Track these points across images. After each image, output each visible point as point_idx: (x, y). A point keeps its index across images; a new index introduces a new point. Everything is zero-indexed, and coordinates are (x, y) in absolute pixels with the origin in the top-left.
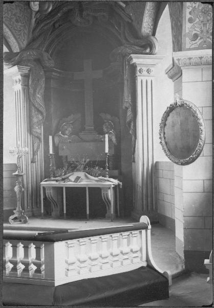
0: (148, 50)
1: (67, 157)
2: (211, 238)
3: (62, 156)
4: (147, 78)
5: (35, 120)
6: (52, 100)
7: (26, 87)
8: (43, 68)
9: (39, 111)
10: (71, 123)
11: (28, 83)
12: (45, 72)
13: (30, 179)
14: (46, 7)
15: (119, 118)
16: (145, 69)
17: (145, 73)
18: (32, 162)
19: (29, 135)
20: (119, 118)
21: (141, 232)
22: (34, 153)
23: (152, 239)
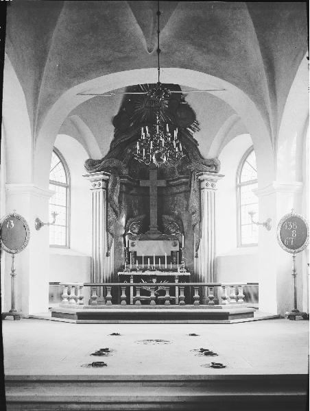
1: (135, 252)
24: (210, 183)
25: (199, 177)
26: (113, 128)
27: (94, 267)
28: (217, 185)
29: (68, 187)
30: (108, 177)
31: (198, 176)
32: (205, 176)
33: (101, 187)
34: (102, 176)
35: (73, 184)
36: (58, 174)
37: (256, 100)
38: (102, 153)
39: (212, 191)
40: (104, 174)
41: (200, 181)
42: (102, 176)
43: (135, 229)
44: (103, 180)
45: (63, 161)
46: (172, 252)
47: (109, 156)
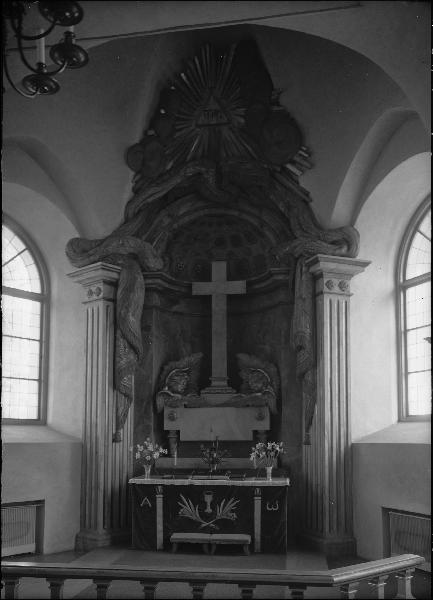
0: (344, 250)
1: (178, 432)
2: (214, 21)
3: (168, 432)
4: (340, 297)
5: (123, 362)
6: (154, 328)
7: (111, 304)
8: (142, 271)
9: (132, 347)
10: (185, 372)
11: (115, 294)
12: (145, 277)
13: (110, 481)
14: (181, 213)
15: (276, 365)
16: (336, 282)
17: (336, 289)
18: (114, 441)
19: (111, 391)
20: (276, 365)
21: (224, 379)
22: (119, 424)
23: (160, 199)
33: (101, 296)
44: (105, 282)
46: (256, 432)
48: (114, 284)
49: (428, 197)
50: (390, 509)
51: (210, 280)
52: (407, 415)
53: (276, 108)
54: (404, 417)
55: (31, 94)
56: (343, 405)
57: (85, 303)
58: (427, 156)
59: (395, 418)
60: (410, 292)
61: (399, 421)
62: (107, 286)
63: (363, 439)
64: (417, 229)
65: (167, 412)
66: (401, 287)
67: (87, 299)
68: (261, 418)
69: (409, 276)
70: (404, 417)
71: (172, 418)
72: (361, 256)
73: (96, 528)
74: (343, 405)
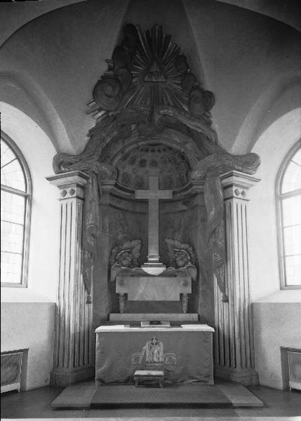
1: (126, 295)
3: (118, 295)
24: (240, 190)
25: (225, 181)
26: (87, 139)
27: (56, 314)
28: (249, 194)
29: (28, 198)
30: (85, 181)
31: (222, 179)
32: (234, 179)
33: (75, 195)
34: (76, 179)
35: (35, 196)
36: (13, 175)
37: (144, 232)
38: (74, 148)
39: (244, 203)
40: (80, 175)
41: (227, 187)
42: (77, 177)
43: (125, 259)
44: (78, 186)
45: (20, 156)
46: (181, 295)
47: (86, 153)
48: (83, 187)
49: (298, 141)
50: (287, 349)
51: (160, 200)
52: (286, 285)
53: (206, 118)
54: (284, 287)
55: (182, 282)
56: (246, 262)
57: (61, 200)
58: (299, 110)
59: (278, 287)
60: (285, 201)
61: (281, 289)
62: (80, 189)
63: (260, 299)
64: (290, 160)
65: (118, 279)
66: (279, 197)
67: (62, 198)
68: (185, 284)
69: (283, 192)
70: (284, 287)
71: (122, 284)
72: (256, 175)
73: (225, 365)
74: (246, 262)
